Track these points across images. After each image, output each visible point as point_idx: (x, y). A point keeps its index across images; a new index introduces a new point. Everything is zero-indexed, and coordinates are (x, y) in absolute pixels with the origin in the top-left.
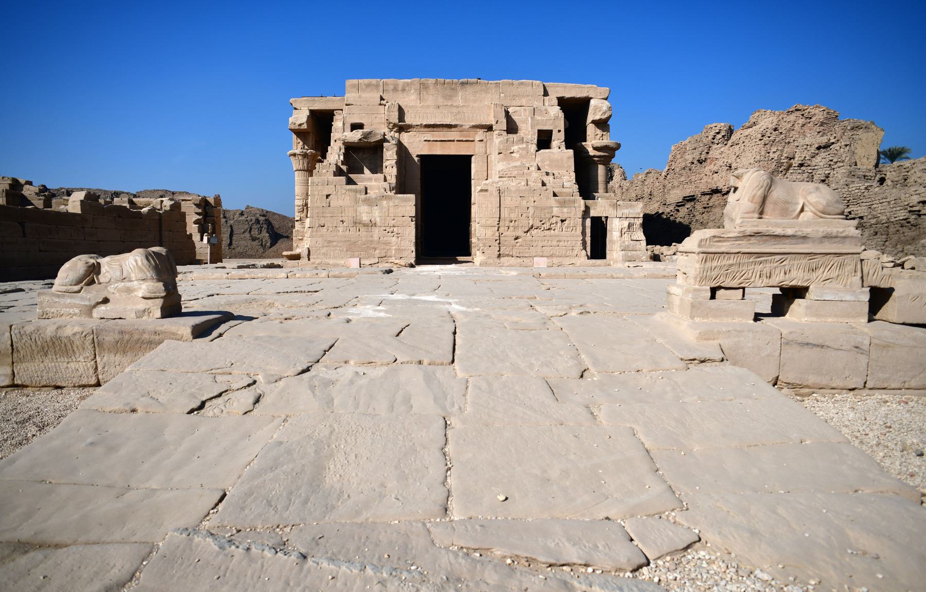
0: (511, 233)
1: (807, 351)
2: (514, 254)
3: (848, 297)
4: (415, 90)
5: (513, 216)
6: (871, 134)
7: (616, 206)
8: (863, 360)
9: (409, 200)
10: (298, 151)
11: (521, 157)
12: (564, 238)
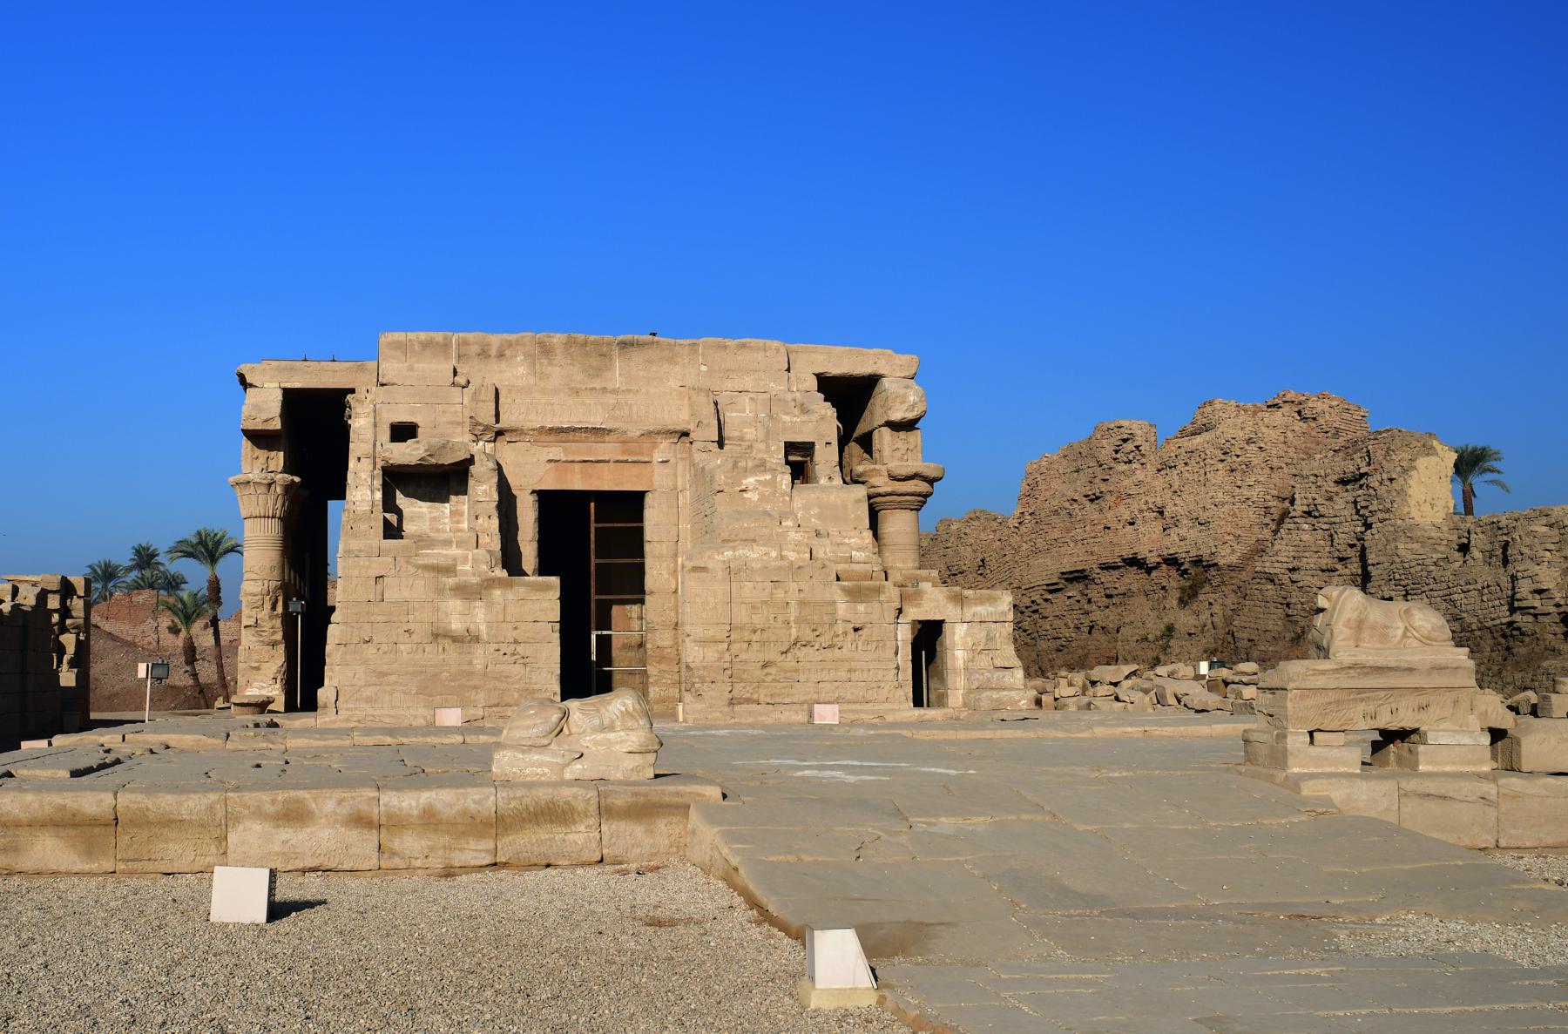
0: (754, 656)
1: (1428, 804)
2: (762, 698)
3: (1467, 740)
4: (526, 355)
5: (758, 620)
6: (1433, 459)
7: (960, 600)
8: (1492, 813)
9: (548, 587)
10: (255, 475)
11: (763, 498)
12: (859, 665)
